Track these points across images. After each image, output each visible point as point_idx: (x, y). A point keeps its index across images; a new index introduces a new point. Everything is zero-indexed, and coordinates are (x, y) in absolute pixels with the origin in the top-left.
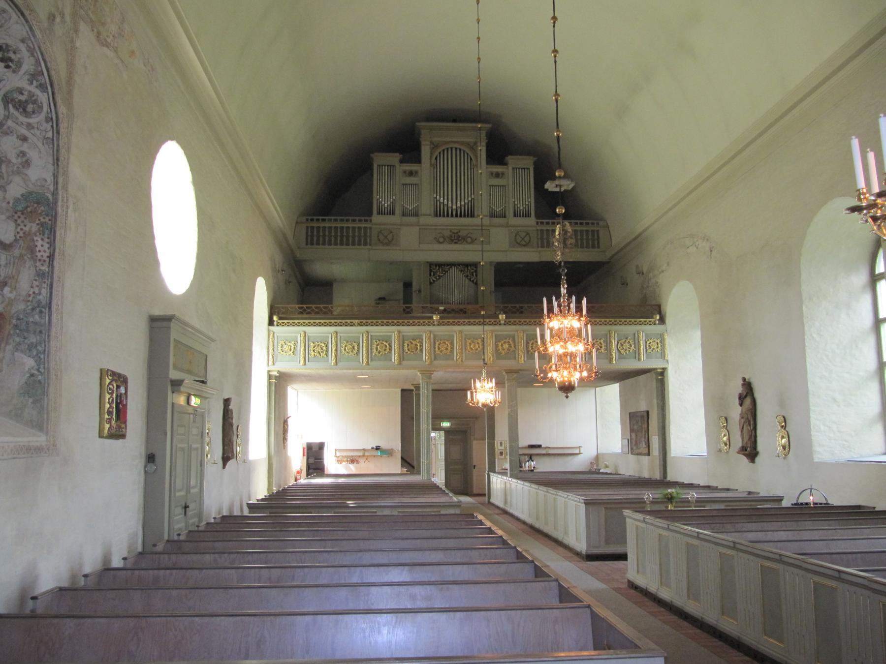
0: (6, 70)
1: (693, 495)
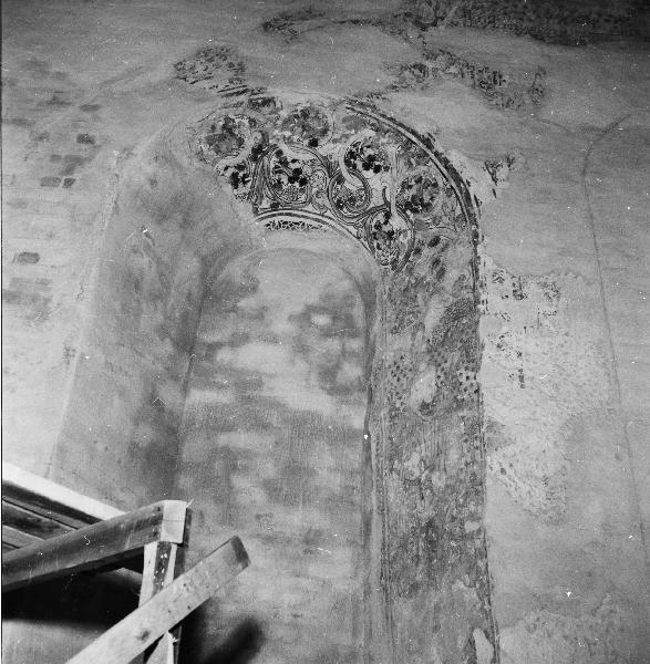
0: (379, 174)
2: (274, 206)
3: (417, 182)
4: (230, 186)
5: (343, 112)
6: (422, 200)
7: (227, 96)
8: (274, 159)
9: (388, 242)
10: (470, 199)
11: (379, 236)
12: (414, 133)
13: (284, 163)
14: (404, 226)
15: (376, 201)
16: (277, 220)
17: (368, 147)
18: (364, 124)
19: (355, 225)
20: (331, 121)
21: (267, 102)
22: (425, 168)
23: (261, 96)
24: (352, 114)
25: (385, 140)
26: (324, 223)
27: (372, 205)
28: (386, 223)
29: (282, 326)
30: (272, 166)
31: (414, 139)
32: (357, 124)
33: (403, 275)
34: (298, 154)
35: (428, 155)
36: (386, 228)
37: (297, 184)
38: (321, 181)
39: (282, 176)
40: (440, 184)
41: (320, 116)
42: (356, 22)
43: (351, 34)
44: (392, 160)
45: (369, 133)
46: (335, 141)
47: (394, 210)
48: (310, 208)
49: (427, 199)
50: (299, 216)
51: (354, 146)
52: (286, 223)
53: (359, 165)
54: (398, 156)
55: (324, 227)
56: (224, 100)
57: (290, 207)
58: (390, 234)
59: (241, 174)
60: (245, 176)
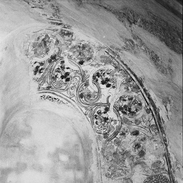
0: (109, 88)
1: (176, 86)
2: (48, 88)
3: (129, 99)
4: (33, 72)
5: (103, 53)
6: (130, 109)
8: (59, 64)
9: (103, 123)
11: (99, 118)
12: (135, 75)
13: (63, 68)
14: (115, 118)
16: (47, 94)
17: (108, 74)
19: (86, 108)
20: (95, 54)
21: (69, 34)
22: (136, 95)
25: (118, 74)
26: (69, 102)
27: (99, 102)
28: (105, 113)
29: (45, 161)
30: (57, 67)
31: (134, 78)
32: (107, 61)
33: (112, 143)
34: (71, 66)
35: (140, 89)
36: (105, 116)
37: (64, 80)
39: (59, 74)
40: (143, 105)
42: (105, 8)
43: (105, 13)
45: (111, 67)
46: (92, 65)
48: (65, 93)
49: (133, 109)
50: (58, 96)
52: (50, 97)
53: (100, 80)
55: (69, 104)
56: (50, 25)
58: (106, 119)
59: (40, 68)
60: (42, 69)
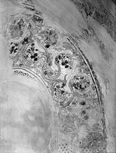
0: (66, 69)
3: (81, 78)
4: (9, 51)
7: (28, 8)
8: (30, 46)
9: (60, 94)
10: (102, 94)
13: (33, 49)
14: (70, 91)
15: (62, 77)
16: (19, 70)
17: (67, 57)
18: (70, 48)
19: (48, 82)
20: (59, 40)
21: (40, 20)
23: (39, 16)
24: (68, 41)
27: (58, 78)
30: (28, 49)
31: (86, 62)
32: (68, 47)
34: (39, 48)
35: (89, 71)
36: (62, 89)
37: (33, 59)
38: (43, 62)
39: (29, 54)
41: (56, 37)
44: (74, 66)
46: (56, 49)
47: (67, 84)
48: (33, 70)
50: (27, 71)
51: (62, 54)
52: (22, 72)
53: (61, 62)
54: (77, 66)
55: (36, 79)
57: (29, 66)
58: (63, 92)
59: (15, 48)
60: (16, 49)
